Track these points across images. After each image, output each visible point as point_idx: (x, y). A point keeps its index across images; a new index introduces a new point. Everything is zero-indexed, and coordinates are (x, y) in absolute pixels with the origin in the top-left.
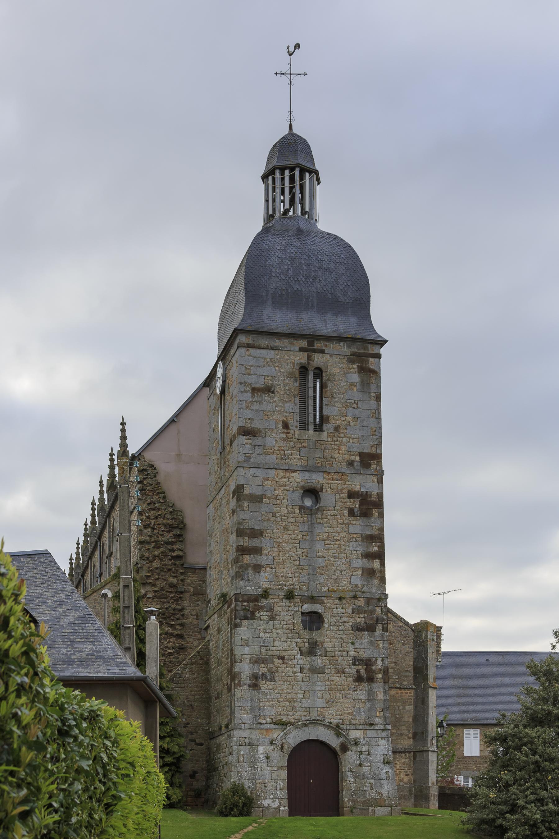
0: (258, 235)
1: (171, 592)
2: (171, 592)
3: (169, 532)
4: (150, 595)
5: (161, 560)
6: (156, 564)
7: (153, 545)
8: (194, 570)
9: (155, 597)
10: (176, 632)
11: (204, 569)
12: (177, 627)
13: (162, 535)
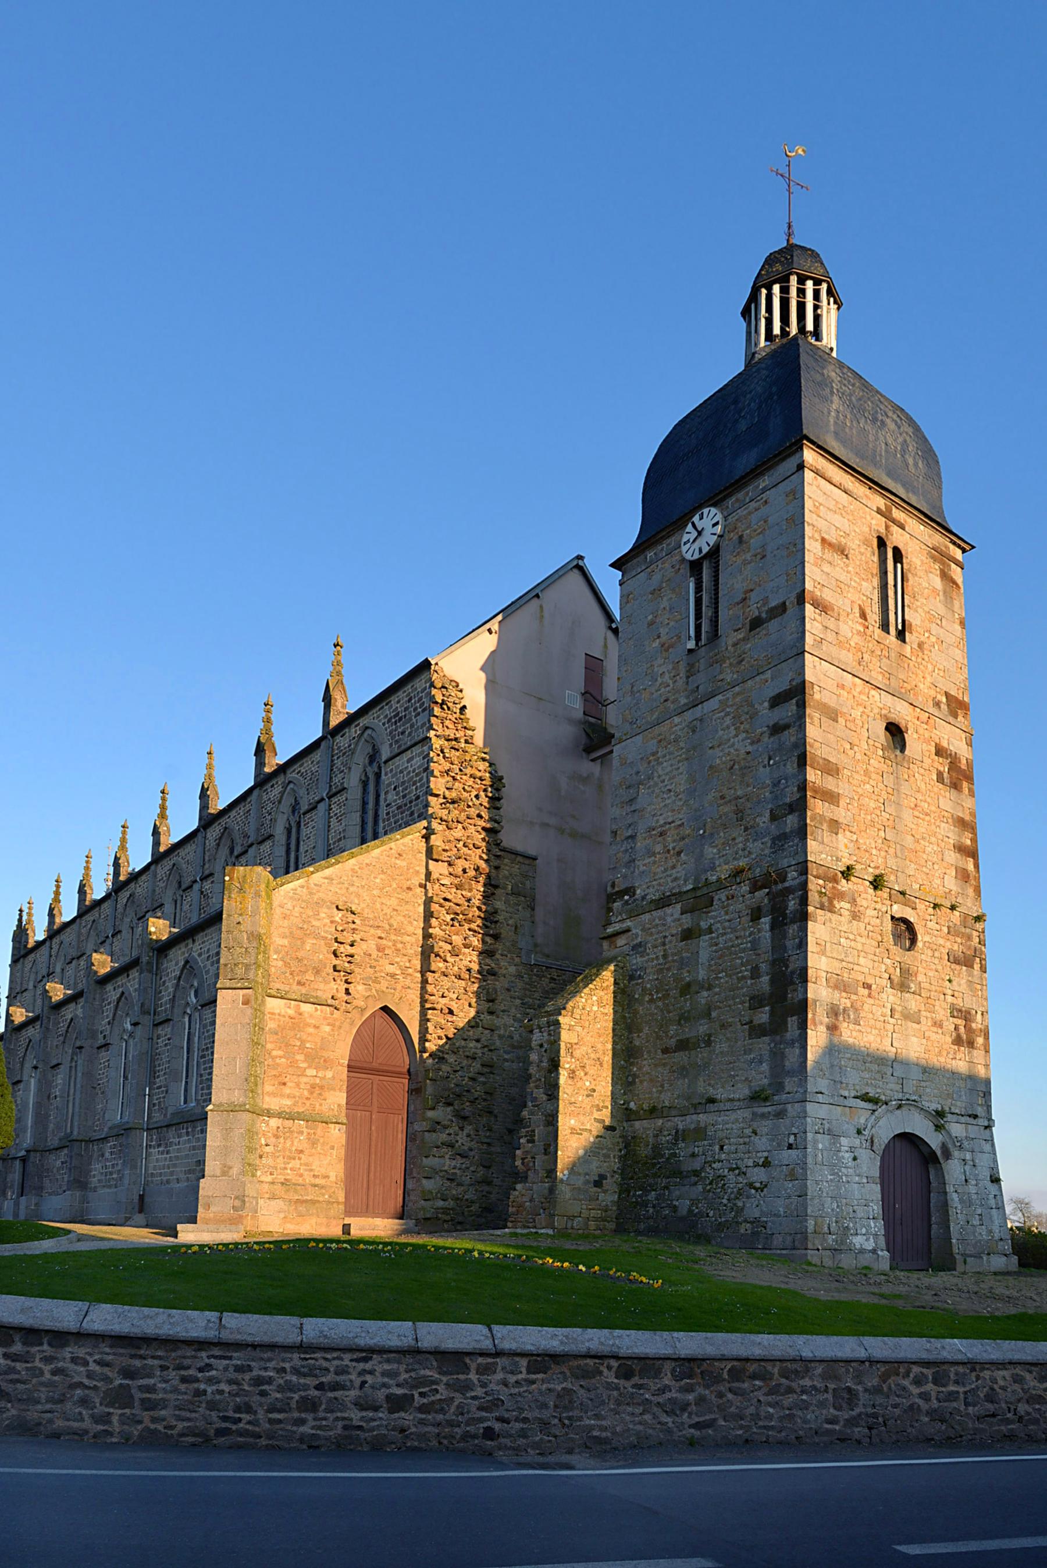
4: (446, 881)
6: (458, 832)
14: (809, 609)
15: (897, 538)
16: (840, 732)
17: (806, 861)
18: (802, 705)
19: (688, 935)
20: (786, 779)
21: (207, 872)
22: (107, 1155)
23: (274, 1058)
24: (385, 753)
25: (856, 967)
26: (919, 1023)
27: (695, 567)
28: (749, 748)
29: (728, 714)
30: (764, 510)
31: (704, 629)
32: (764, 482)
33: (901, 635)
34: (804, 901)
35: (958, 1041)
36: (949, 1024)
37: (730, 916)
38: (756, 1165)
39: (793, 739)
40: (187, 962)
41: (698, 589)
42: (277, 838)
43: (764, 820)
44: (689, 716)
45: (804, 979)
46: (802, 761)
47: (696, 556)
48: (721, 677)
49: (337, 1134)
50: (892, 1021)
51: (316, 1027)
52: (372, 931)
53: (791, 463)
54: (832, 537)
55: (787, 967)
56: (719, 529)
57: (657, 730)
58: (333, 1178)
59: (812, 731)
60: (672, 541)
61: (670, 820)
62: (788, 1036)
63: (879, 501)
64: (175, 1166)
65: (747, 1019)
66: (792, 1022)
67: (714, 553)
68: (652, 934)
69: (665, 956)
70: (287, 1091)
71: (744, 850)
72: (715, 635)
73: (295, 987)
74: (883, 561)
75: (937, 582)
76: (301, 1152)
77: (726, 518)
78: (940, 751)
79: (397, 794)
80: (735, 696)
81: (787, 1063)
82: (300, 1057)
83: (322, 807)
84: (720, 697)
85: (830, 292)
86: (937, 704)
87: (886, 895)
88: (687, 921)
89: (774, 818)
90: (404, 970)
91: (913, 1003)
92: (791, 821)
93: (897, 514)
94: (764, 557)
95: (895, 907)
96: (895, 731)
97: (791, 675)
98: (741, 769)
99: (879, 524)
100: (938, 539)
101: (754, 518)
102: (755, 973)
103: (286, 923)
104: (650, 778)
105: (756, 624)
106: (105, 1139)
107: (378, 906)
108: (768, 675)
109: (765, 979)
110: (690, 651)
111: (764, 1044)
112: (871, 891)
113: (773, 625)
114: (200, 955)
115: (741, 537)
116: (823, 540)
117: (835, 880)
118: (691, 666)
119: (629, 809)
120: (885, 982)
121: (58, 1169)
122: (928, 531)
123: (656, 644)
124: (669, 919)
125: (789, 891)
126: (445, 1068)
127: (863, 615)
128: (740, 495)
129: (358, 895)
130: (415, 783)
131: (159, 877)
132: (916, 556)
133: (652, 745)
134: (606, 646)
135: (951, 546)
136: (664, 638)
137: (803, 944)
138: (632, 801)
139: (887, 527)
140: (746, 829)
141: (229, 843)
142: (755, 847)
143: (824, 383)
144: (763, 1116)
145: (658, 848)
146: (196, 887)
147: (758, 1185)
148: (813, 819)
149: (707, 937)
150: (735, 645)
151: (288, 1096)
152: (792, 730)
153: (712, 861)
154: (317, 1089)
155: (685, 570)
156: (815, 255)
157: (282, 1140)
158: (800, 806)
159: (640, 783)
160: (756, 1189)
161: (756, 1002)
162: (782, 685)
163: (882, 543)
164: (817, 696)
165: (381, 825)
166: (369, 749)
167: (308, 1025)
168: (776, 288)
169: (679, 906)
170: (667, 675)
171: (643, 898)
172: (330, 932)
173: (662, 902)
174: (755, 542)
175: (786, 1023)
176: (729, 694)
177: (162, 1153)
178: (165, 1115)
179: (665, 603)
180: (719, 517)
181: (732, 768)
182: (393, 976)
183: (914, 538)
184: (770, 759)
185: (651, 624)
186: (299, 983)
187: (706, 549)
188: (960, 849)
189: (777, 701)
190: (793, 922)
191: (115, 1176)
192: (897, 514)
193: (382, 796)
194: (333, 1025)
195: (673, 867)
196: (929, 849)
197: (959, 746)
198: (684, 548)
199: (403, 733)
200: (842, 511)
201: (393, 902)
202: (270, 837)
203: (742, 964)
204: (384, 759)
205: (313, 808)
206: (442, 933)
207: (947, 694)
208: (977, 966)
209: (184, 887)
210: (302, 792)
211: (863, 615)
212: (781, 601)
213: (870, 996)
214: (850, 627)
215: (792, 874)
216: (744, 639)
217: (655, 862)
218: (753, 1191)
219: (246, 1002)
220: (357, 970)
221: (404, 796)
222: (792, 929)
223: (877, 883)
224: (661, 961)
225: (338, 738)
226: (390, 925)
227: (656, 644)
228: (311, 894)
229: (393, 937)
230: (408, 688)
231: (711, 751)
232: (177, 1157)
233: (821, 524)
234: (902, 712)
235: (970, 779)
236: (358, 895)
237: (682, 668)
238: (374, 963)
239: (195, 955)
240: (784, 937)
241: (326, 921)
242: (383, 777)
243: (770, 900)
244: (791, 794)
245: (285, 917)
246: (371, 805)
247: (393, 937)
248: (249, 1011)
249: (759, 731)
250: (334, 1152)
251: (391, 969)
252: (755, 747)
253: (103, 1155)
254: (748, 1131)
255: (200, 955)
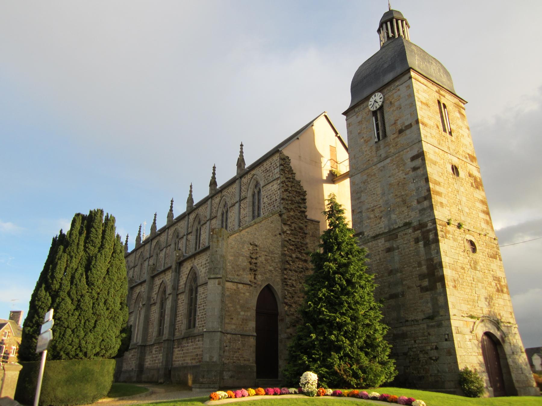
0: (51, 248)
1: (300, 232)
2: (300, 232)
3: (298, 196)
4: (289, 232)
5: (294, 211)
6: (292, 213)
7: (290, 202)
8: (312, 221)
9: (291, 234)
10: (303, 258)
11: (319, 222)
12: (304, 255)
13: (295, 197)
14: (421, 125)
15: (443, 101)
16: (436, 170)
17: (435, 219)
18: (424, 160)
19: (389, 250)
20: (422, 187)
21: (189, 231)
22: (154, 352)
23: (228, 307)
24: (262, 183)
25: (459, 261)
26: (483, 283)
27: (374, 113)
28: (405, 176)
29: (394, 164)
30: (399, 93)
31: (381, 134)
32: (397, 83)
33: (450, 133)
34: (436, 235)
35: (498, 290)
36: (493, 284)
37: (406, 241)
38: (432, 349)
39: (422, 172)
40: (192, 268)
41: (377, 120)
42: (218, 217)
43: (415, 203)
44: (379, 165)
45: (441, 267)
46: (427, 180)
47: (375, 109)
48: (390, 151)
49: (252, 341)
50: (474, 283)
51: (244, 294)
52: (263, 253)
53: (406, 77)
54: (424, 101)
55: (433, 262)
56: (382, 100)
57: (366, 171)
58: (251, 361)
59: (429, 169)
60: (365, 104)
61: (376, 205)
62: (438, 291)
63: (435, 88)
64: (186, 357)
65: (418, 284)
66: (439, 285)
67: (381, 107)
68: (373, 251)
69: (380, 259)
70: (234, 321)
71: (408, 215)
72: (385, 135)
73: (236, 277)
74: (440, 108)
75: (458, 115)
76: (239, 349)
77: (384, 96)
78: (470, 175)
79: (268, 199)
80: (396, 157)
81: (439, 303)
82: (238, 307)
83: (237, 205)
84: (390, 158)
85: (406, 24)
86: (466, 158)
87: (463, 231)
88: (388, 245)
89: (419, 202)
90: (275, 268)
91: (479, 275)
92: (426, 203)
93: (442, 92)
94: (400, 108)
95: (467, 235)
96: (455, 170)
97: (417, 150)
98: (402, 184)
99: (437, 96)
100: (456, 100)
101: (395, 95)
102: (420, 265)
103: (232, 250)
104: (365, 189)
105: (401, 131)
106: (153, 345)
107: (265, 243)
108: (409, 149)
109: (424, 267)
110: (376, 142)
111: (428, 295)
112: (458, 230)
113: (408, 132)
114: (198, 265)
115: (391, 102)
116: (421, 102)
117: (445, 226)
118: (377, 147)
119: (358, 201)
120: (469, 267)
121: (130, 359)
122: (452, 97)
123: (362, 140)
124: (380, 244)
125: (430, 231)
126: (292, 309)
127: (438, 127)
128: (389, 88)
129: (258, 239)
130: (275, 194)
131: (169, 234)
132: (450, 107)
133: (365, 177)
134: (336, 143)
135: (460, 103)
136: (365, 138)
137: (438, 252)
138: (359, 198)
139: (440, 97)
140: (408, 207)
141: (198, 220)
142: (413, 214)
143: (412, 51)
144: (432, 326)
145: (372, 216)
146: (185, 237)
147: (434, 358)
148: (435, 202)
149: (397, 251)
150: (394, 139)
151: (234, 324)
152: (421, 169)
153: (395, 220)
154: (245, 320)
155: (371, 114)
156: (399, 13)
157: (232, 344)
158: (428, 197)
159: (362, 191)
160: (434, 360)
161: (422, 277)
162: (415, 152)
163: (439, 102)
164: (428, 156)
165: (262, 211)
166: (255, 183)
167: (241, 293)
168: (389, 24)
169: (383, 239)
170: (368, 151)
171: (368, 236)
172: (247, 254)
173: (376, 237)
174: (397, 104)
175: (436, 285)
176: (394, 157)
177: (180, 351)
178: (181, 334)
179: (364, 126)
180: (382, 96)
181: (398, 184)
182: (271, 271)
183: (448, 100)
184: (414, 180)
185: (359, 133)
186: (237, 275)
187: (378, 107)
188: (484, 212)
189: (413, 158)
190: (433, 243)
191: (157, 361)
192: (442, 92)
193: (262, 200)
194: (250, 293)
195: (379, 223)
196: (474, 213)
197: (475, 173)
198: (370, 107)
199: (269, 176)
200: (424, 91)
201: (270, 241)
202: (216, 217)
203: (414, 262)
204: (262, 186)
205: (234, 205)
206: (288, 253)
207: (468, 154)
208: (498, 259)
209: (180, 237)
210: (228, 200)
211: (438, 127)
212: (409, 123)
213: (465, 273)
214: (434, 132)
215: (430, 224)
216: (397, 137)
217: (371, 222)
218: (432, 361)
219: (219, 284)
220: (258, 269)
221: (271, 200)
222: (433, 246)
223: (459, 226)
224: (378, 261)
225: (243, 179)
226: (270, 250)
227: (362, 140)
228: (241, 239)
229: (270, 255)
230: (270, 160)
231: (389, 179)
232: (187, 353)
233: (420, 96)
234: (456, 162)
235: (481, 185)
236: (258, 239)
237: (374, 149)
238: (264, 266)
239: (196, 264)
240: (430, 249)
241: (246, 250)
242: (262, 193)
243: (422, 235)
244: (424, 193)
245: (232, 248)
246: (256, 203)
247: (270, 255)
248: (220, 288)
249: (408, 170)
250: (252, 349)
251: (271, 268)
252: (407, 176)
253: (152, 352)
254: (426, 334)
255: (198, 265)
